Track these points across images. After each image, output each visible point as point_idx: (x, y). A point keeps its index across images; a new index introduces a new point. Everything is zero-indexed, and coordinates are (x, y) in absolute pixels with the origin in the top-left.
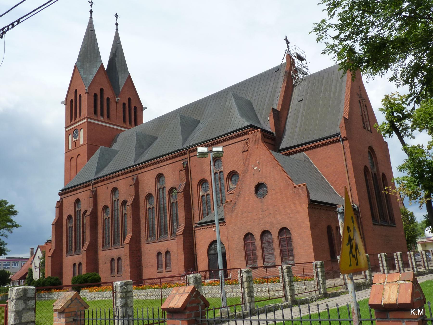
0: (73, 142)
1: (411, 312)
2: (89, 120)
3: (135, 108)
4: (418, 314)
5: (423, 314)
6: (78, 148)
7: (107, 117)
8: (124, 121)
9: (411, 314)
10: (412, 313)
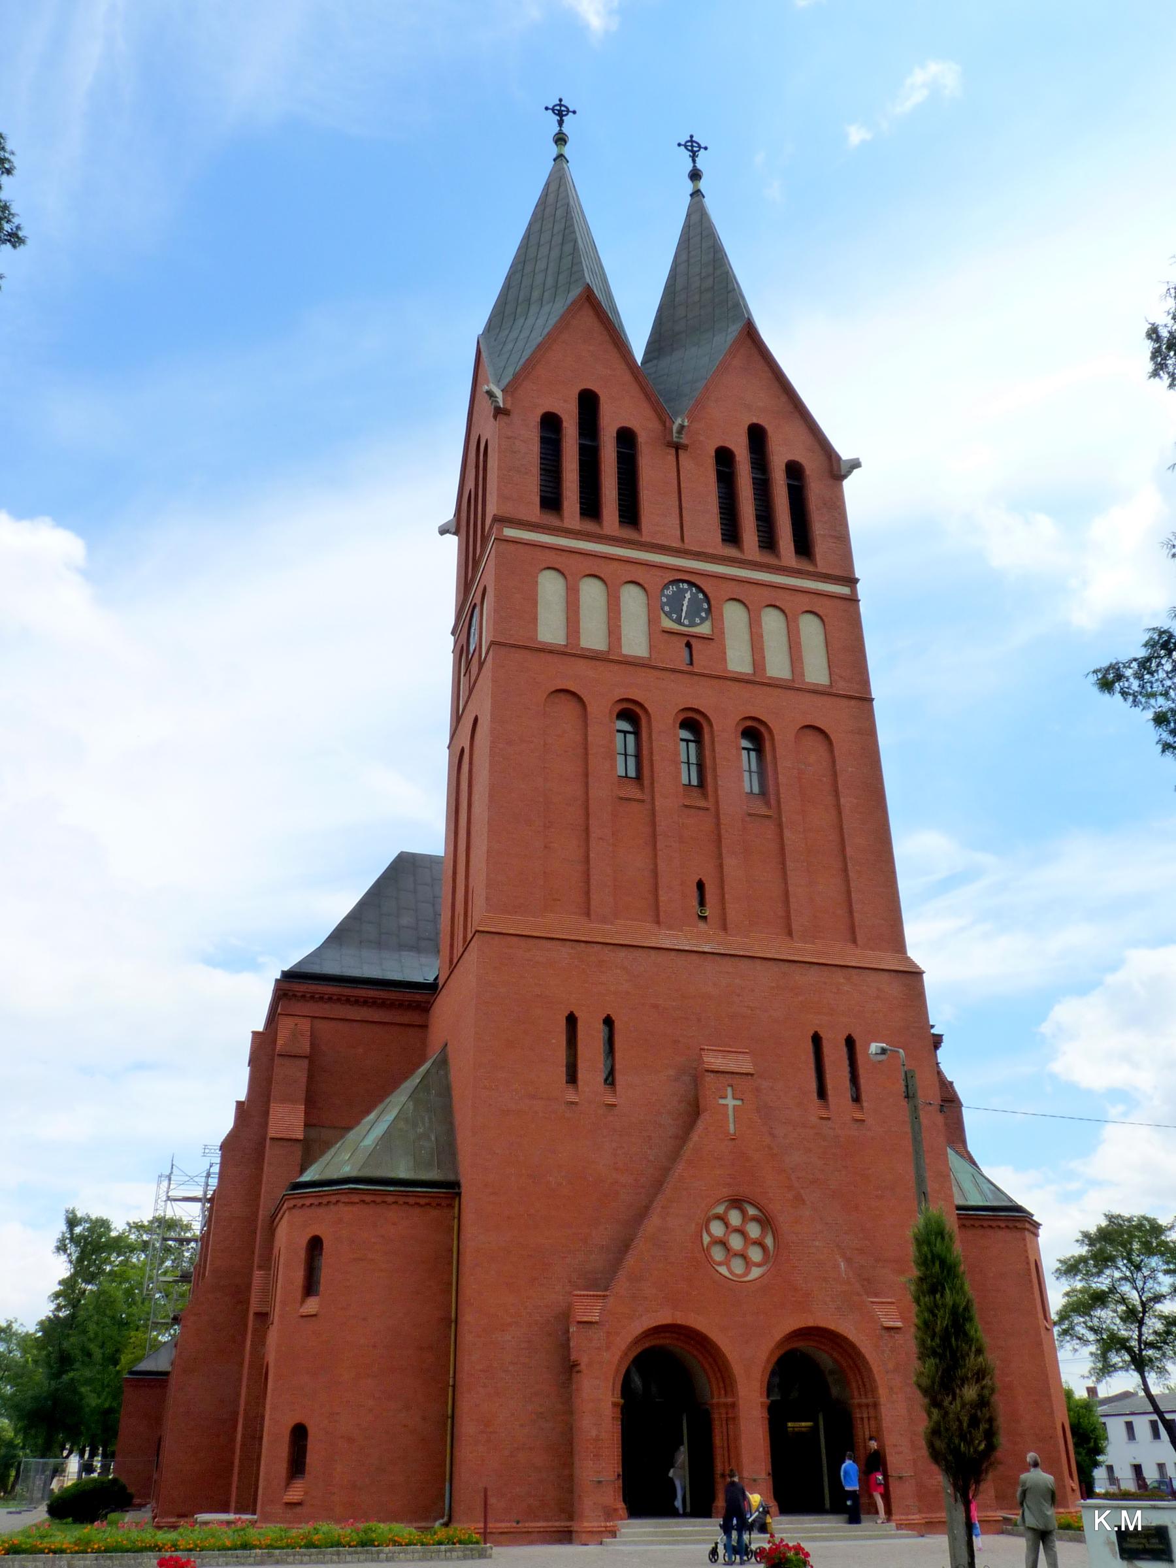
1: (1097, 1521)
3: (794, 471)
7: (617, 519)
8: (731, 535)
9: (1097, 1529)
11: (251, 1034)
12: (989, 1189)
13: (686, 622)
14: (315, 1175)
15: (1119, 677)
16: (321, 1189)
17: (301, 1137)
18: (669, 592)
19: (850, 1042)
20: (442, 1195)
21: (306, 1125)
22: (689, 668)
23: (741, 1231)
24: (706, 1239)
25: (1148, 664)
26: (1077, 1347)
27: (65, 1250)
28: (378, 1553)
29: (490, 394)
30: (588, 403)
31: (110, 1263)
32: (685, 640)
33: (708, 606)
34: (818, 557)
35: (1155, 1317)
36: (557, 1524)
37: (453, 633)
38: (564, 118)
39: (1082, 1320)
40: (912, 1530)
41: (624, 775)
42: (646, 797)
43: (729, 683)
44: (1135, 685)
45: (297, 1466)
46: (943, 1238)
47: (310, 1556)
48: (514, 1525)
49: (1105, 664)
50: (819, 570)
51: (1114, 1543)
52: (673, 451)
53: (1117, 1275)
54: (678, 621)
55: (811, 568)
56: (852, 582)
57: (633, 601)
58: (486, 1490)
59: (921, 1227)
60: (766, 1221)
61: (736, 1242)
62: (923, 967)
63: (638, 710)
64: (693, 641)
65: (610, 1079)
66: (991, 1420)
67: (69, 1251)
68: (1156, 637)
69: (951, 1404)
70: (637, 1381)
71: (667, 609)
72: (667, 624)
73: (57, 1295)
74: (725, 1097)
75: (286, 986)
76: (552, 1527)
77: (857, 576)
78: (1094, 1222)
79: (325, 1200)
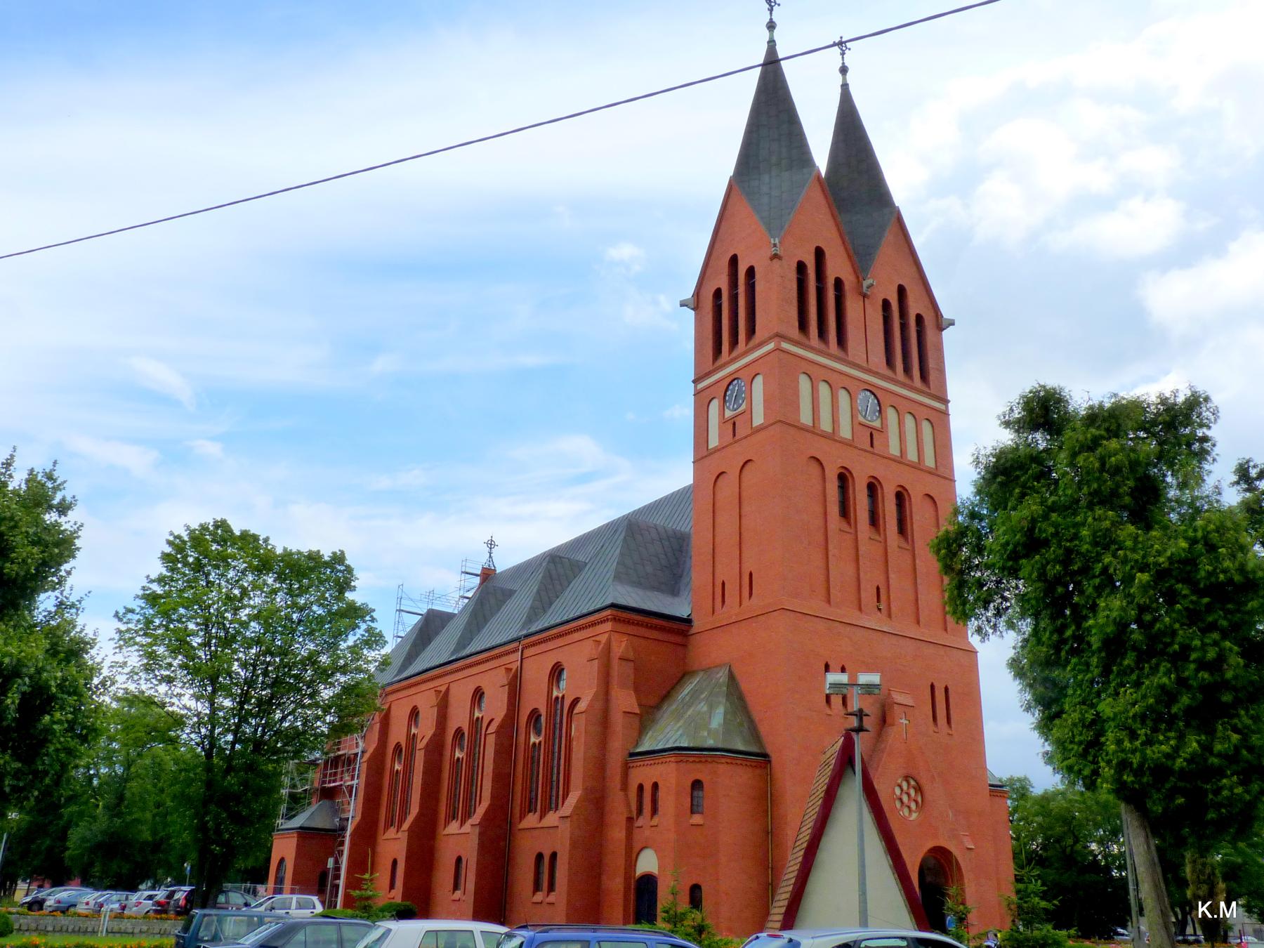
0: (723, 421)
1: (1200, 910)
2: (785, 345)
4: (1221, 916)
5: (1235, 916)
6: (741, 439)
9: (1200, 916)
10: (1203, 912)
13: (869, 418)
34: (849, 349)
42: (852, 531)
50: (932, 391)
56: (945, 401)
60: (919, 789)
61: (905, 798)
62: (978, 650)
64: (874, 432)
79: (703, 760)
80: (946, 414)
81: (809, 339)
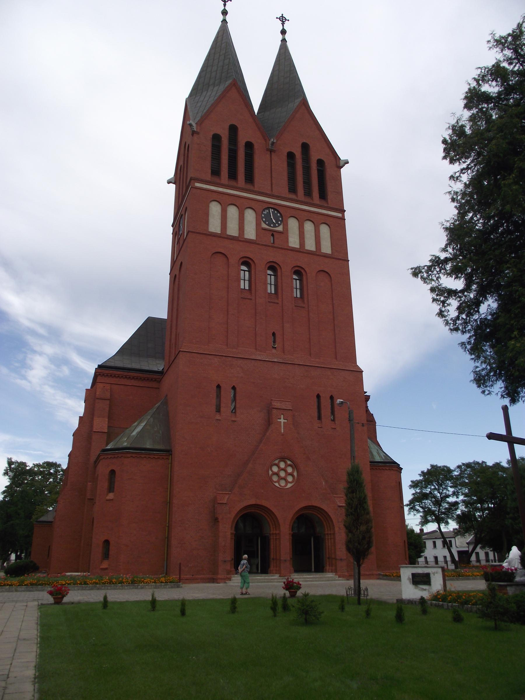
3: (320, 163)
8: (293, 189)
11: (85, 390)
12: (384, 455)
14: (112, 446)
15: (421, 272)
16: (115, 452)
17: (106, 431)
18: (265, 213)
19: (332, 398)
20: (164, 455)
21: (109, 427)
22: (273, 245)
23: (284, 470)
24: (270, 473)
25: (431, 268)
26: (415, 513)
27: (7, 474)
28: (138, 586)
29: (191, 125)
30: (233, 130)
31: (27, 480)
32: (271, 233)
33: (283, 220)
34: (329, 200)
35: (446, 503)
36: (208, 576)
37: (173, 226)
38: (226, 3)
39: (418, 503)
40: (343, 578)
41: (244, 288)
43: (289, 251)
44: (425, 275)
45: (106, 555)
46: (358, 473)
47: (111, 587)
48: (192, 576)
49: (415, 266)
50: (329, 206)
51: (411, 579)
52: (269, 153)
53: (433, 487)
54: (269, 225)
55: (326, 205)
57: (250, 216)
58: (180, 564)
59: (350, 469)
60: (295, 466)
61: (282, 474)
63: (250, 261)
64: (274, 233)
65: (234, 411)
66: (370, 537)
67: (9, 474)
68: (434, 258)
69: (356, 532)
70: (241, 525)
71: (264, 219)
72: (264, 226)
73: (4, 492)
74: (280, 419)
75: (100, 371)
76: (206, 577)
77: (345, 209)
78: (426, 467)
79: (116, 456)
80: (343, 219)
81: (312, 199)
